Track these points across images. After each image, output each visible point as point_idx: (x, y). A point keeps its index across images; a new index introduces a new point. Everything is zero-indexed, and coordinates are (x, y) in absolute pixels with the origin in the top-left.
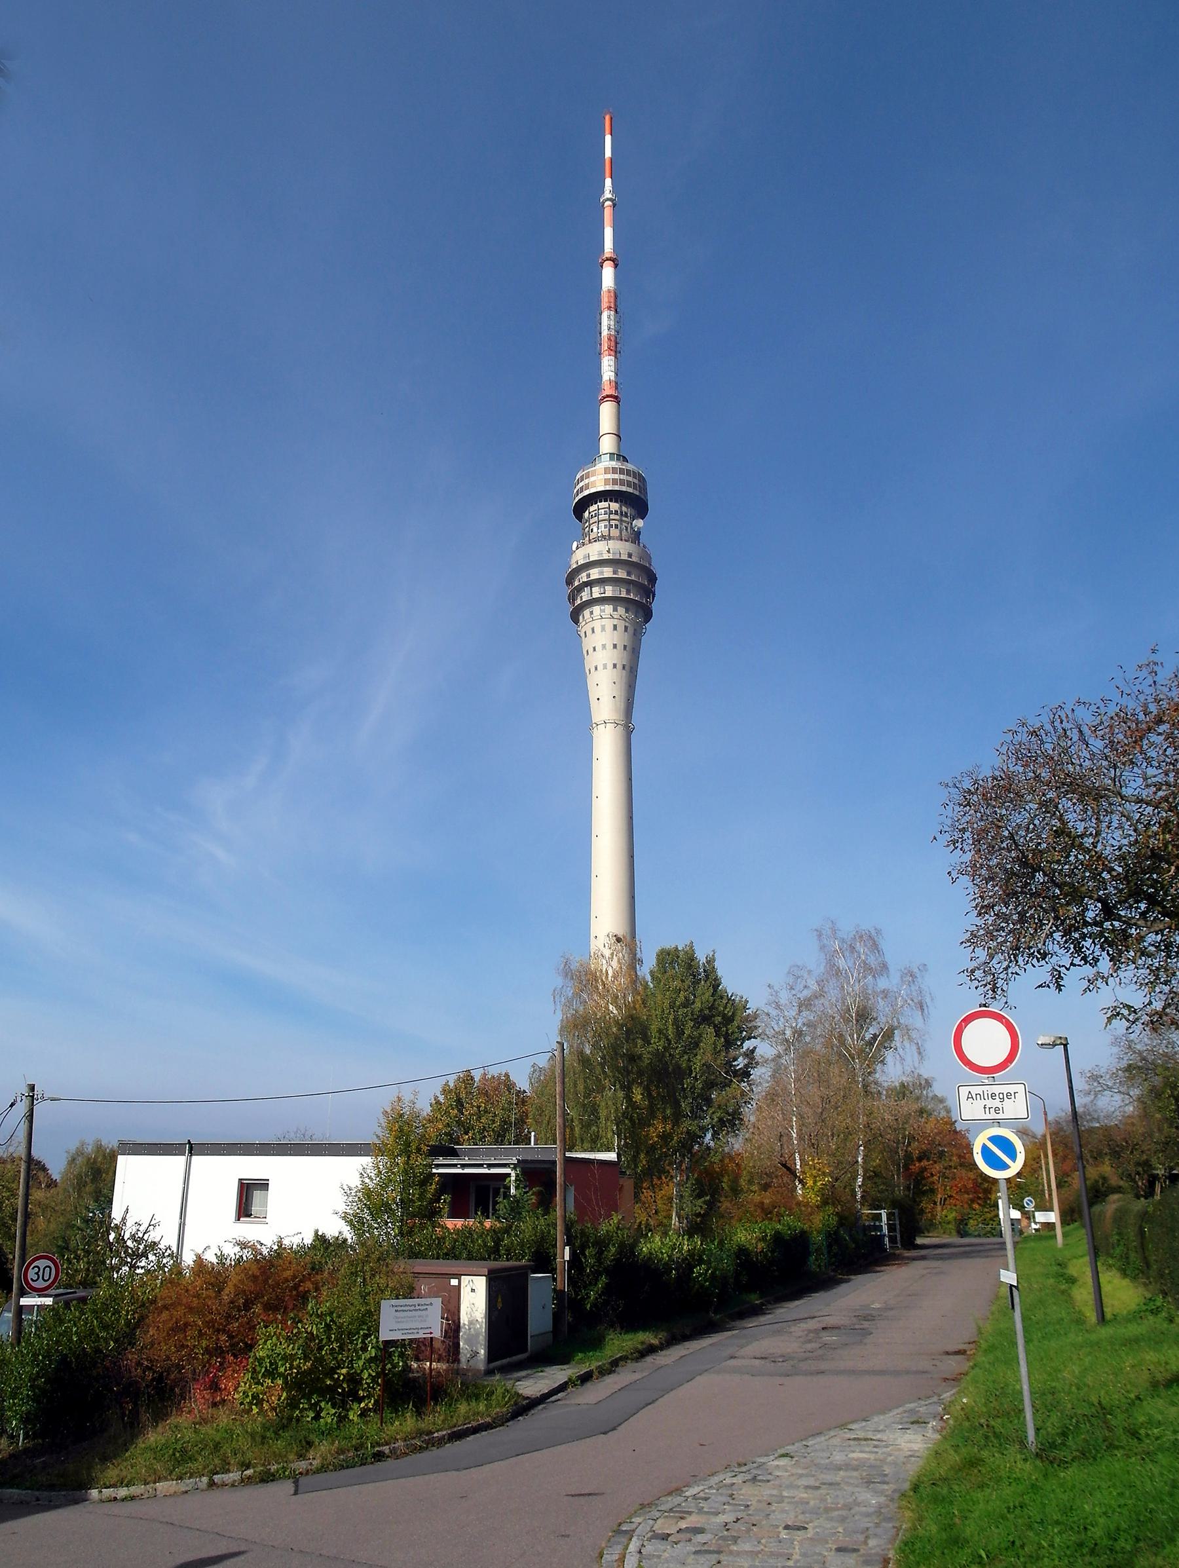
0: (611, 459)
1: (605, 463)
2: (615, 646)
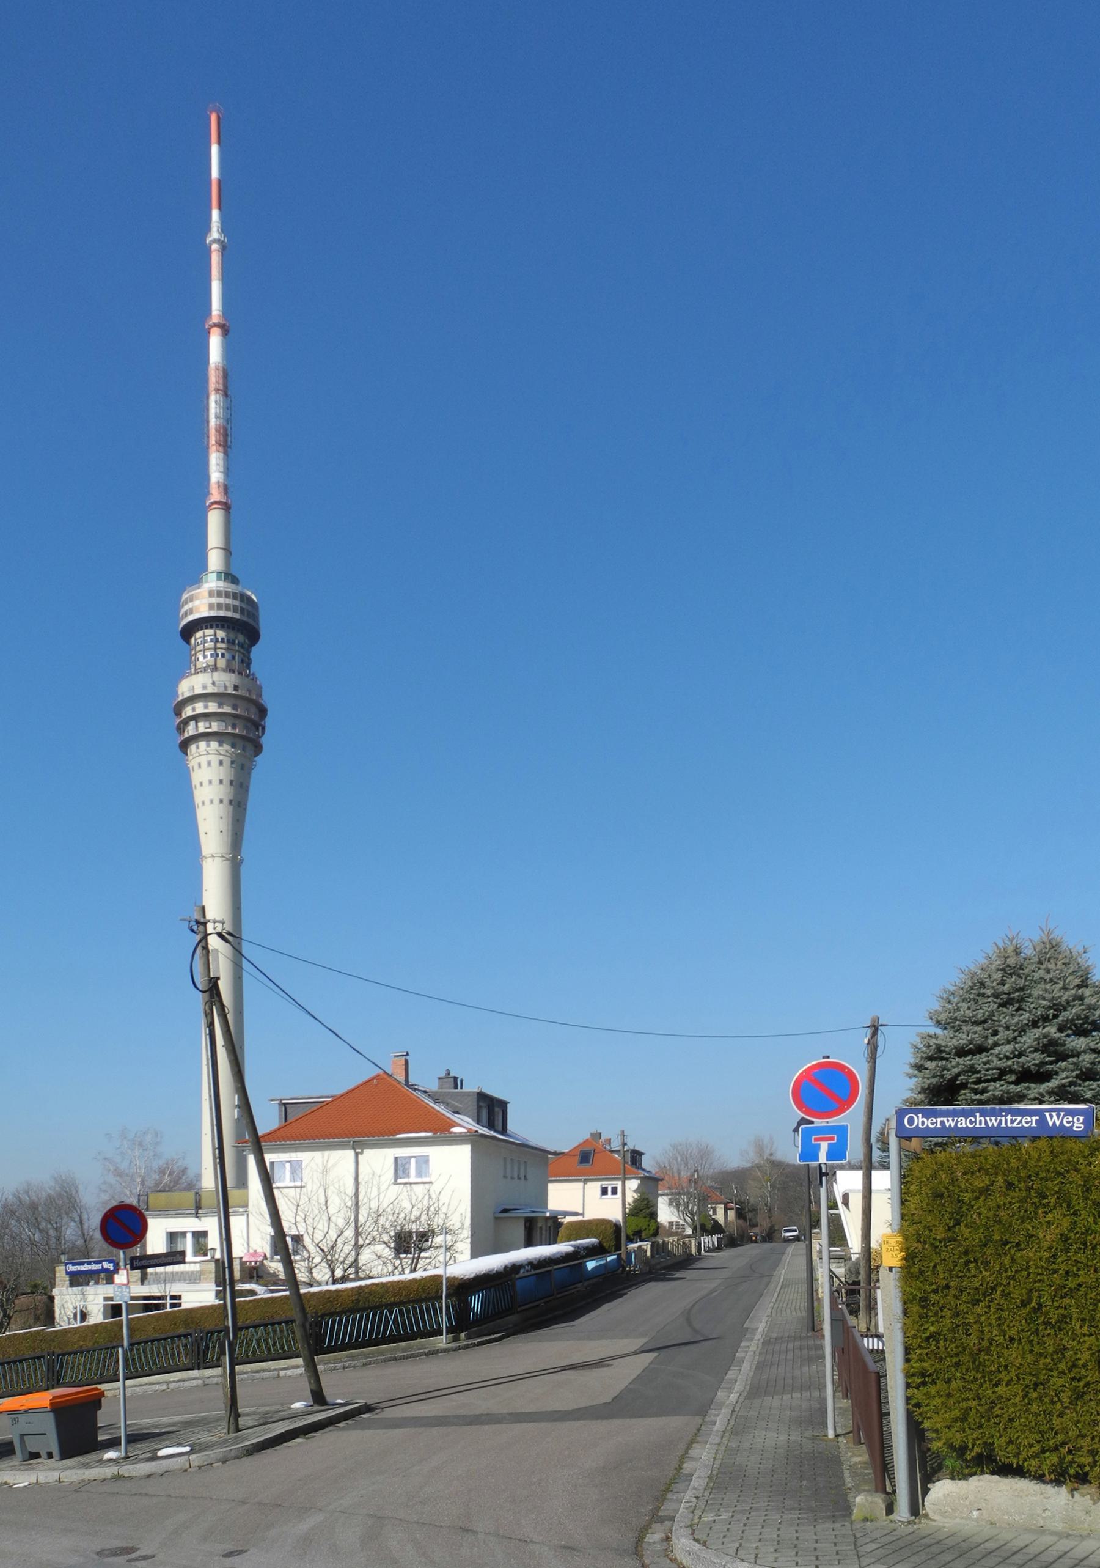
0: (219, 579)
1: (212, 582)
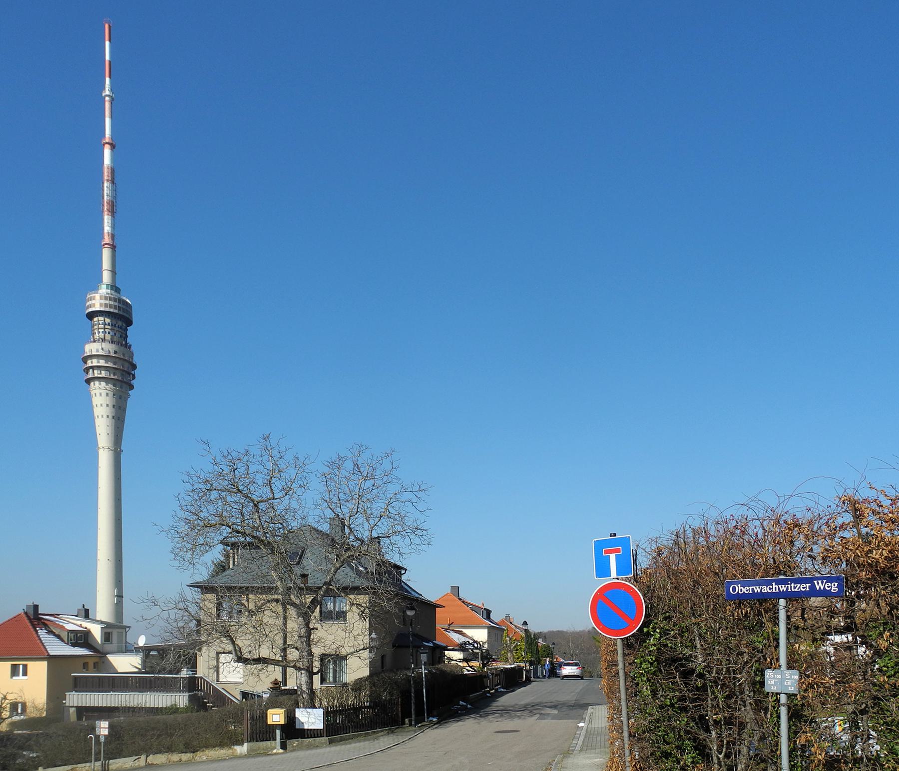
0: (107, 288)
1: (104, 290)
2: (107, 405)
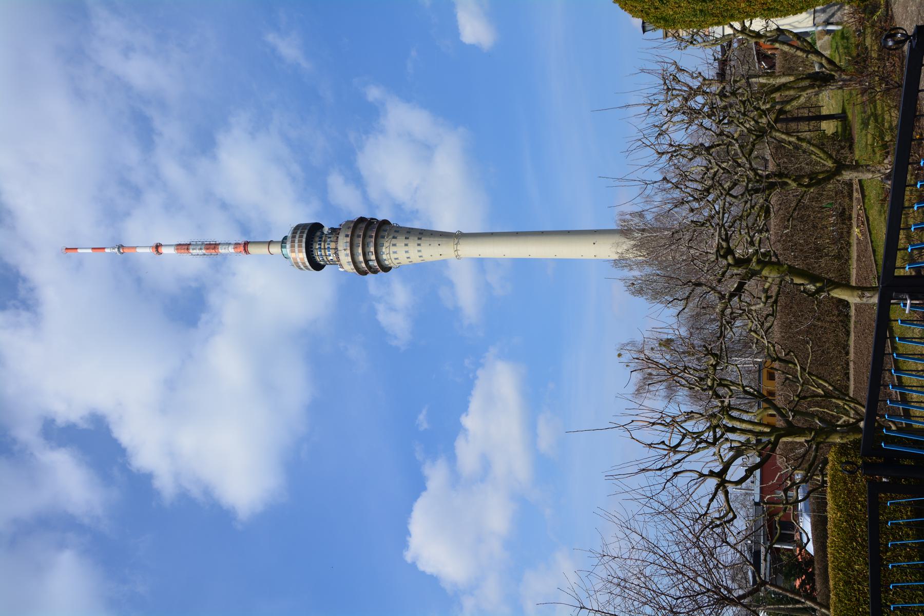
0: (285, 247)
2: (406, 245)
